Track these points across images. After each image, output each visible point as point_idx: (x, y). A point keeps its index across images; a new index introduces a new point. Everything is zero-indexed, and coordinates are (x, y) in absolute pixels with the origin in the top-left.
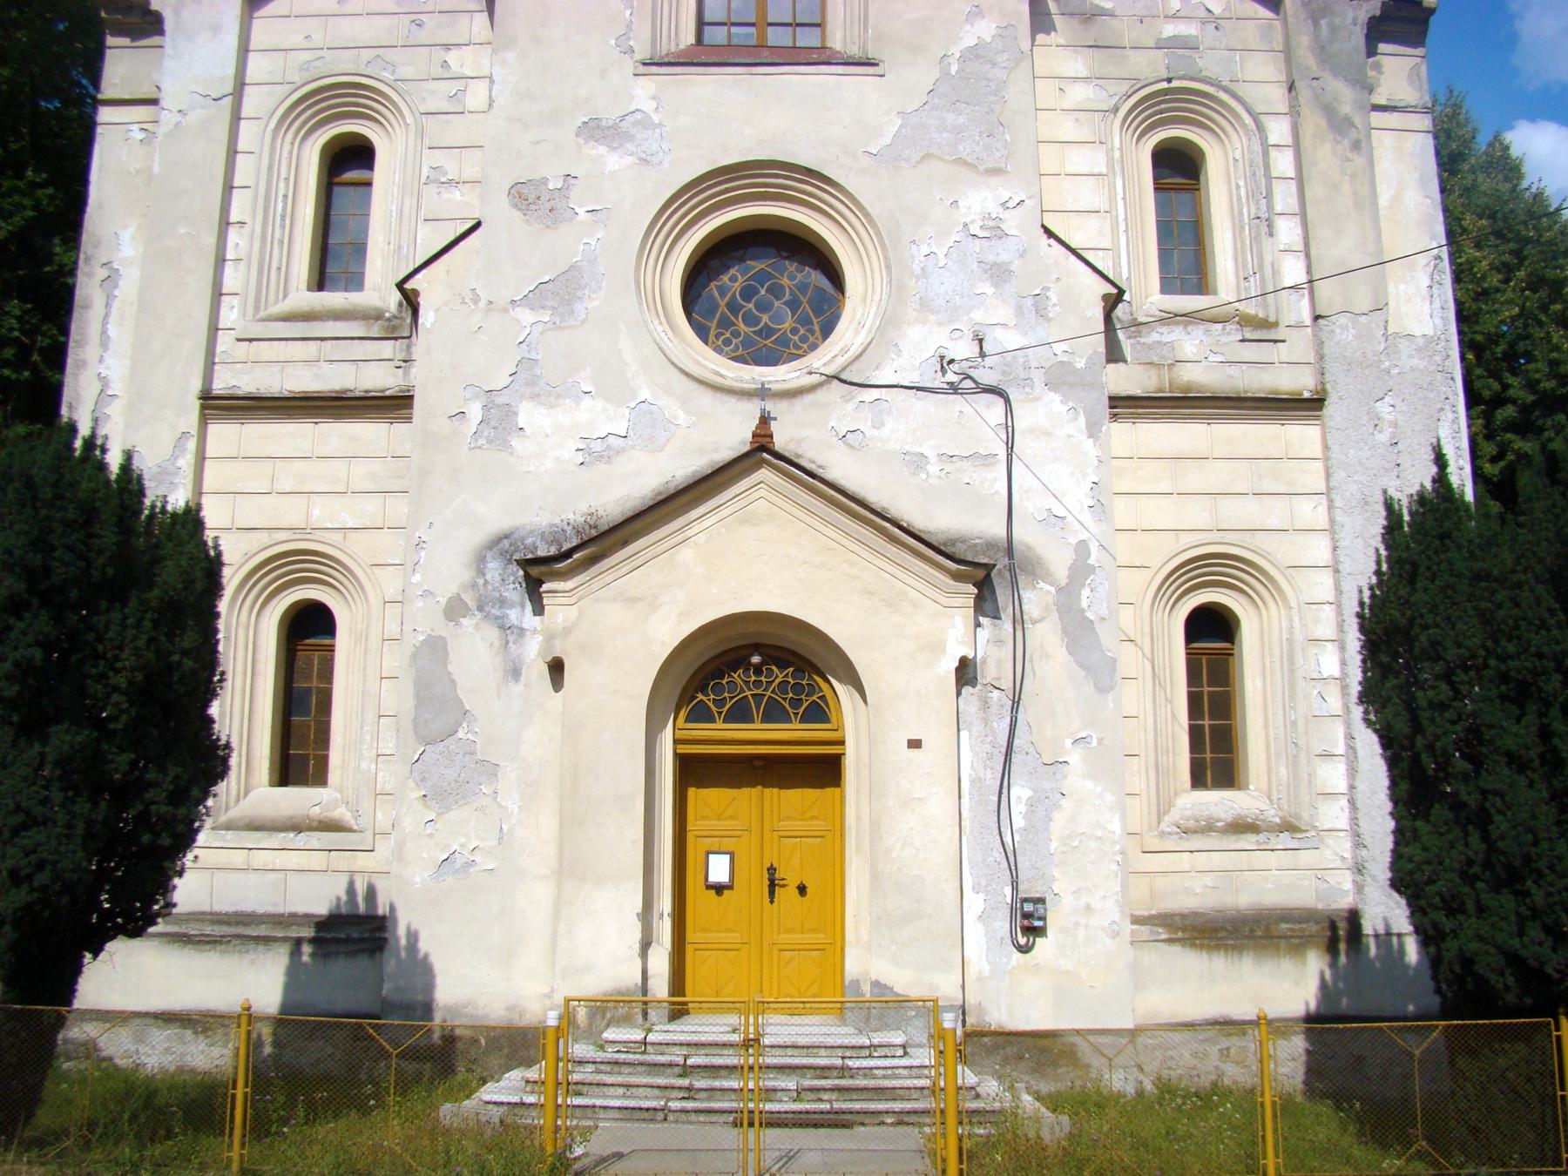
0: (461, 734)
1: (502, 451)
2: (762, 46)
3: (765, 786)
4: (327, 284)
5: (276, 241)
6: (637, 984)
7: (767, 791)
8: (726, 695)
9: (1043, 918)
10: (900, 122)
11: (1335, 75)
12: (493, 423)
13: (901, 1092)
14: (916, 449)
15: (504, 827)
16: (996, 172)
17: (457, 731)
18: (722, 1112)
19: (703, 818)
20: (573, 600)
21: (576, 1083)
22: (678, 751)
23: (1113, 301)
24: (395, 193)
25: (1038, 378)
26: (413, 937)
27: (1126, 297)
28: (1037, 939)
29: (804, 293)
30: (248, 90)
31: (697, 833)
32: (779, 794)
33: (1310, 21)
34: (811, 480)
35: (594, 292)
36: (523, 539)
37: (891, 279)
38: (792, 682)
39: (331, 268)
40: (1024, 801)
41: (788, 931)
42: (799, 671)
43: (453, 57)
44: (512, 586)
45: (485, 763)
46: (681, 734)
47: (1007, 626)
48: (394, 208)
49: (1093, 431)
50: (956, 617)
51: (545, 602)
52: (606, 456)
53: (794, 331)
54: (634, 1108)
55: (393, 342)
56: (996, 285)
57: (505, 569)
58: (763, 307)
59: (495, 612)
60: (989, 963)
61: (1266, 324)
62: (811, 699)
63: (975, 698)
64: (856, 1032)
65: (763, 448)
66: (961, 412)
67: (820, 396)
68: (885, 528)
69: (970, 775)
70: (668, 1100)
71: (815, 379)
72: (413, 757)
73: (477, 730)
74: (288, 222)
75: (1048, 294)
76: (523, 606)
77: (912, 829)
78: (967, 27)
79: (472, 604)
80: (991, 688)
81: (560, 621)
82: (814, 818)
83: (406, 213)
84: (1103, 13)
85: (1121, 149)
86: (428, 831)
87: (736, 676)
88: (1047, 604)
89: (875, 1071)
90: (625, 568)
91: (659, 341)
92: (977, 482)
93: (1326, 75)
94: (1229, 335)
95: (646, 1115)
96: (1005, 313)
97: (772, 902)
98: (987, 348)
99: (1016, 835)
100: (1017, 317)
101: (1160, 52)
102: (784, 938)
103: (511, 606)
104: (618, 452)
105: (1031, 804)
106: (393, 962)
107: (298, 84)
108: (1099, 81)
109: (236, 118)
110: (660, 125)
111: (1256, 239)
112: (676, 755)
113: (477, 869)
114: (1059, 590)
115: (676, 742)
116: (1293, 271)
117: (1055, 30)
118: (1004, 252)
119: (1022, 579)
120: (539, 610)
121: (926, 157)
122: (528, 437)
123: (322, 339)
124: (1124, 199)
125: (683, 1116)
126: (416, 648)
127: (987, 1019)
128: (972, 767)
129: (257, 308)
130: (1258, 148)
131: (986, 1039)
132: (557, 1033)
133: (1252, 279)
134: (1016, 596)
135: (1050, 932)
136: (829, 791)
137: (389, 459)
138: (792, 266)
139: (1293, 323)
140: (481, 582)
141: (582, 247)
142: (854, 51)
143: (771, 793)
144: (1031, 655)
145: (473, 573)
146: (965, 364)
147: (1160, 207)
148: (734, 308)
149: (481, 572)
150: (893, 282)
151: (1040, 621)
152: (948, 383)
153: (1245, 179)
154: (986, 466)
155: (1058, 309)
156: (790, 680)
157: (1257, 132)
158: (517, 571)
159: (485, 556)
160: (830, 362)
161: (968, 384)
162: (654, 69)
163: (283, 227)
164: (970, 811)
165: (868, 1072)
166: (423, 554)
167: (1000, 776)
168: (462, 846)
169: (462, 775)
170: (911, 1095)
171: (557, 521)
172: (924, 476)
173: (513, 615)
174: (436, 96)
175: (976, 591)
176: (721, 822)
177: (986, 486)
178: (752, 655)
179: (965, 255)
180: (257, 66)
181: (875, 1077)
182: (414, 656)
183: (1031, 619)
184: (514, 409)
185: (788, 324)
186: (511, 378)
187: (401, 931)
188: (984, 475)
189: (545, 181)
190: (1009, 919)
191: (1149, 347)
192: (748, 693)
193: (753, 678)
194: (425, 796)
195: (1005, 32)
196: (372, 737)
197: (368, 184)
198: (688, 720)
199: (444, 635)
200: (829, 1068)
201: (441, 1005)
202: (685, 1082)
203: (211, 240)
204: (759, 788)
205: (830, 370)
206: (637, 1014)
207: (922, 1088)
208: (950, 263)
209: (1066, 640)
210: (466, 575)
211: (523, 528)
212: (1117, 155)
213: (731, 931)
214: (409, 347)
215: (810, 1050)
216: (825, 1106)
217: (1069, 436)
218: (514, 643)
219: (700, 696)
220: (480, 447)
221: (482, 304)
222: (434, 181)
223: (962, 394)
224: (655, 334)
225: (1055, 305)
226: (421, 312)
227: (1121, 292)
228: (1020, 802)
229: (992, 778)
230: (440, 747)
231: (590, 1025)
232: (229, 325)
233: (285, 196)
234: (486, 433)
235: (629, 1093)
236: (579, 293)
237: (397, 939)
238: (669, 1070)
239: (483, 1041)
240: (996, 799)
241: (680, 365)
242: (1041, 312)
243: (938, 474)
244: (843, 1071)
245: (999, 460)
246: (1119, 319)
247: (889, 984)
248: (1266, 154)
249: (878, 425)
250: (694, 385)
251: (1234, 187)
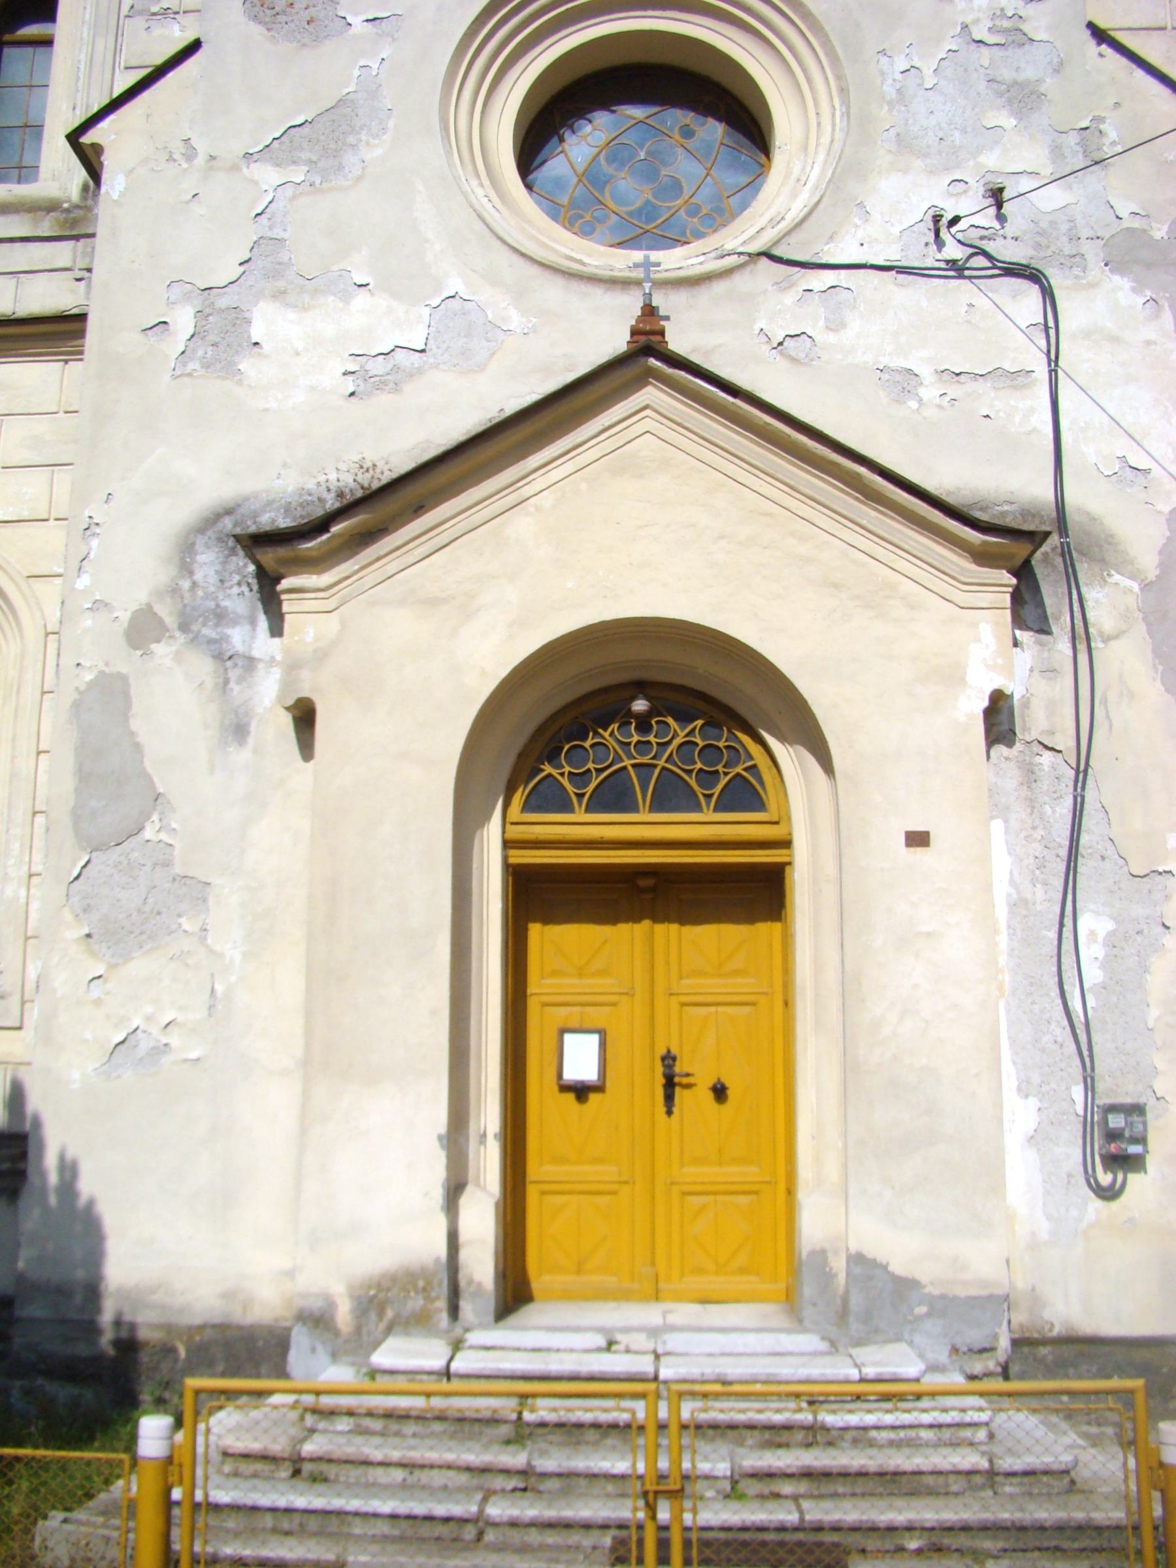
0: (149, 833)
1: (224, 378)
3: (656, 919)
7: (660, 928)
8: (591, 765)
9: (1142, 1140)
13: (929, 1480)
17: (141, 829)
18: (587, 1526)
20: (331, 604)
22: (512, 860)
24: (85, 35)
25: (1093, 253)
26: (69, 1171)
28: (1130, 1176)
32: (680, 934)
34: (730, 399)
35: (375, 136)
37: (848, 107)
38: (701, 744)
40: (1100, 938)
42: (711, 723)
44: (236, 590)
45: (189, 881)
46: (515, 832)
48: (83, 57)
51: (286, 607)
52: (392, 382)
55: (71, 243)
56: (1019, 115)
57: (224, 563)
59: (209, 632)
60: (1049, 1218)
62: (734, 771)
63: (1012, 764)
64: (823, 1346)
65: (649, 350)
67: (742, 282)
68: (858, 476)
69: (1009, 895)
70: (488, 1494)
72: (70, 872)
73: (174, 825)
75: (1102, 127)
77: (916, 986)
79: (170, 621)
80: (1037, 748)
82: (737, 973)
83: (98, 58)
87: (606, 735)
88: (1127, 609)
89: (873, 1433)
91: (477, 207)
92: (1001, 414)
97: (669, 1112)
99: (1089, 997)
100: (1054, 162)
103: (235, 622)
104: (411, 376)
105: (1113, 943)
106: (36, 1213)
114: (1146, 587)
115: (507, 844)
119: (1082, 568)
122: (266, 356)
126: (80, 693)
127: (1047, 1314)
128: (1012, 881)
131: (1043, 1351)
132: (165, 1473)
135: (1151, 1162)
137: (61, 415)
140: (186, 584)
141: (356, 73)
143: (667, 933)
145: (173, 571)
150: (852, 111)
151: (1116, 637)
152: (947, 262)
154: (1015, 388)
156: (698, 740)
158: (245, 566)
159: (193, 544)
160: (752, 238)
164: (1010, 955)
165: (860, 1436)
166: (95, 543)
169: (151, 900)
170: (947, 1485)
171: (311, 485)
172: (913, 404)
173: (237, 637)
178: (633, 698)
179: (966, 70)
182: (77, 705)
183: (1101, 633)
184: (247, 315)
186: (242, 269)
187: (51, 1161)
188: (1013, 403)
190: (1080, 1142)
192: (627, 763)
193: (636, 738)
194: (89, 936)
196: (22, 845)
198: (527, 807)
200: (788, 1427)
202: (516, 1458)
204: (646, 923)
206: (441, 1310)
207: (970, 1473)
208: (943, 83)
209: (1160, 668)
210: (163, 575)
211: (256, 497)
216: (792, 1517)
217: (1148, 343)
218: (239, 682)
219: (548, 769)
220: (189, 375)
221: (200, 160)
222: (142, 13)
223: (970, 278)
224: (472, 197)
226: (105, 177)
228: (1095, 941)
229: (1046, 900)
230: (115, 854)
231: (358, 1330)
234: (200, 353)
236: (351, 139)
237: (43, 1175)
238: (490, 1431)
239: (182, 1352)
243: (938, 401)
244: (815, 1434)
245: (1036, 380)
247: (881, 1257)
249: (836, 325)
250: (535, 270)
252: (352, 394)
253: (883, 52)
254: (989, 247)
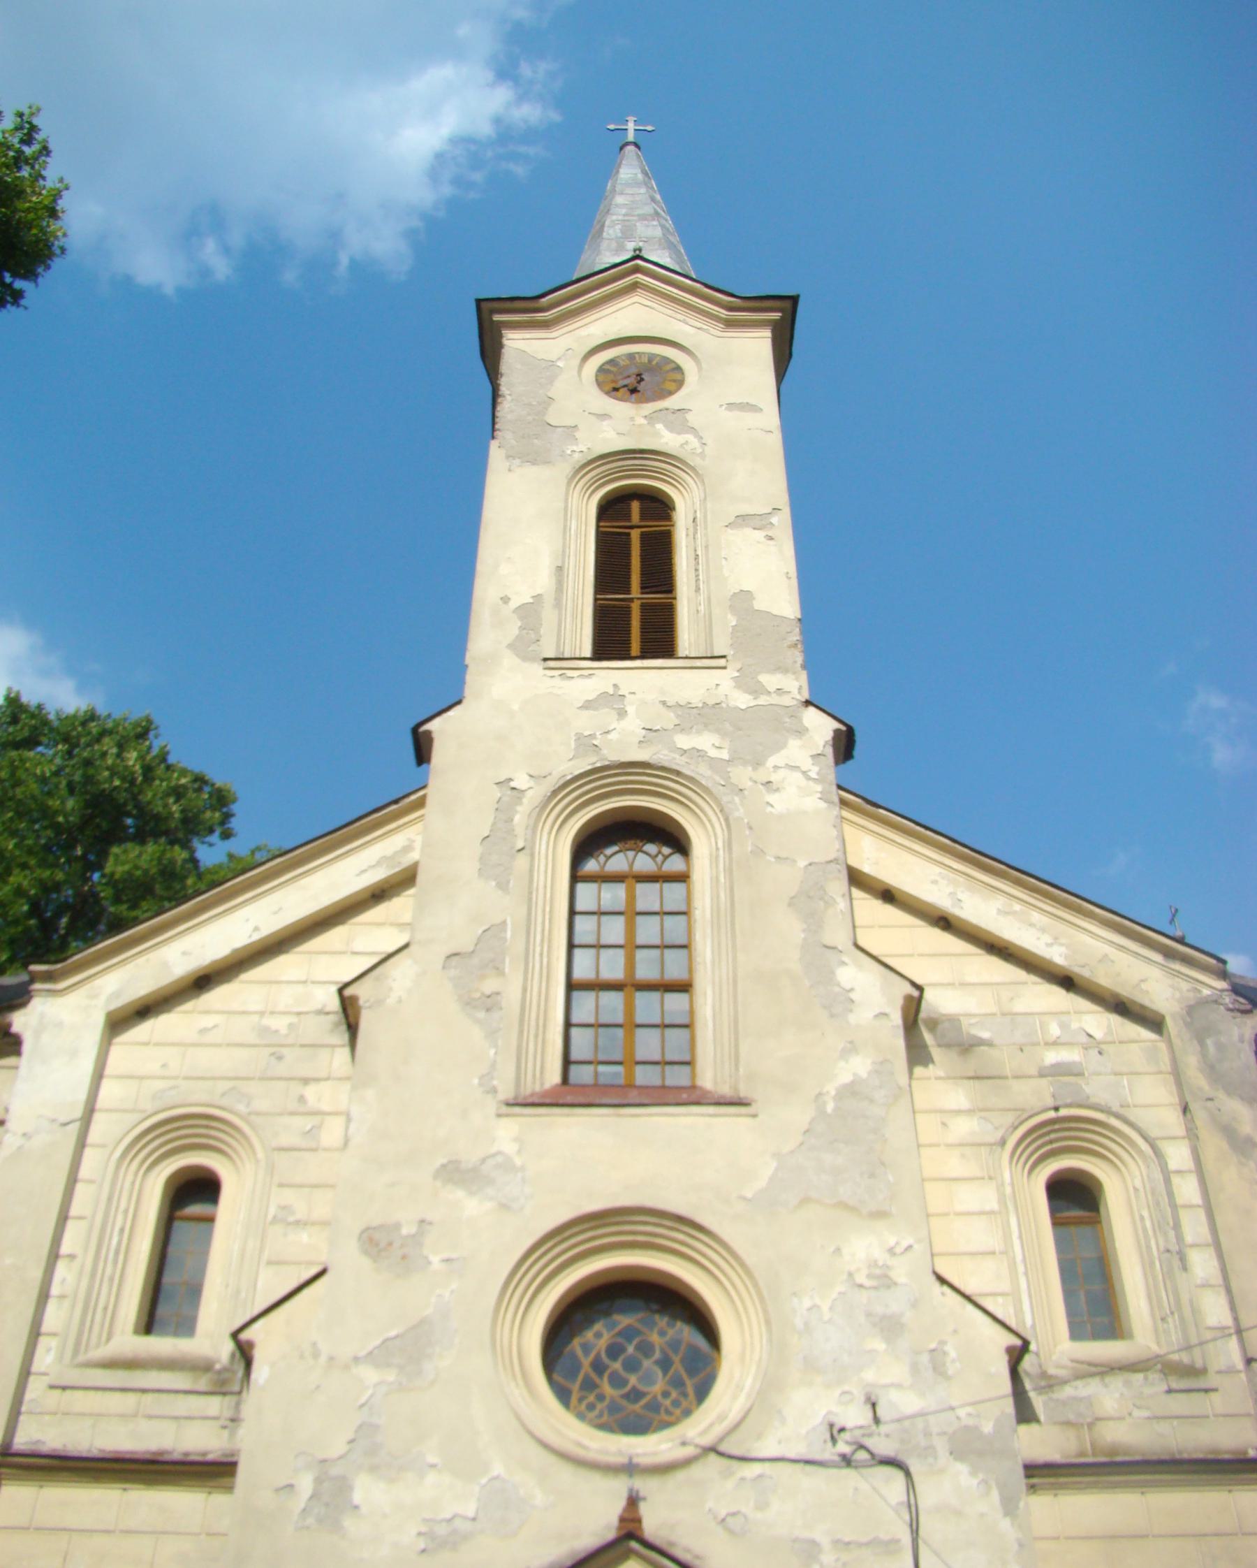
2: (630, 1086)
4: (156, 1326)
5: (106, 1279)
10: (774, 1164)
11: (1229, 1094)
14: (806, 1534)
16: (880, 1215)
23: (1017, 1355)
25: (941, 1446)
27: (1033, 1347)
29: (676, 1351)
30: (97, 1117)
33: (1195, 1042)
39: (162, 1310)
43: (311, 1092)
49: (1009, 1507)
53: (666, 1394)
58: (632, 1366)
61: (1191, 1371)
67: (696, 1471)
71: (689, 1451)
74: (121, 1257)
78: (842, 1064)
84: (982, 1042)
85: (1012, 1185)
93: (1221, 1095)
94: (1152, 1386)
96: (897, 1371)
98: (880, 1412)
101: (1044, 1082)
107: (148, 1113)
108: (983, 1114)
109: (81, 1144)
110: (523, 1168)
111: (1168, 1274)
116: (1215, 1311)
117: (933, 1062)
118: (895, 1303)
121: (805, 1201)
123: (144, 1391)
124: (1020, 1237)
129: (76, 1351)
130: (1158, 1176)
133: (1170, 1320)
138: (662, 1321)
139: (1223, 1368)
142: (725, 1090)
146: (858, 1433)
147: (1062, 1245)
148: (598, 1367)
153: (1149, 1207)
155: (958, 1365)
157: (1155, 1159)
161: (862, 1455)
162: (517, 1110)
163: (115, 1262)
174: (291, 1130)
180: (110, 1091)
185: (658, 1387)
189: (397, 1226)
191: (1064, 1403)
195: (881, 1068)
197: (211, 1220)
203: (37, 1273)
205: (707, 1440)
212: (1008, 1190)
214: (238, 1406)
217: (982, 1515)
221: (323, 1359)
225: (953, 1361)
227: (1025, 1345)
232: (43, 1369)
233: (122, 1230)
241: (537, 1433)
242: (939, 1369)
246: (1028, 1374)
248: (1167, 1181)
249: (762, 1506)
250: (551, 1459)
251: (1137, 1218)
252: (423, 1551)
253: (794, 1294)
254: (869, 1442)
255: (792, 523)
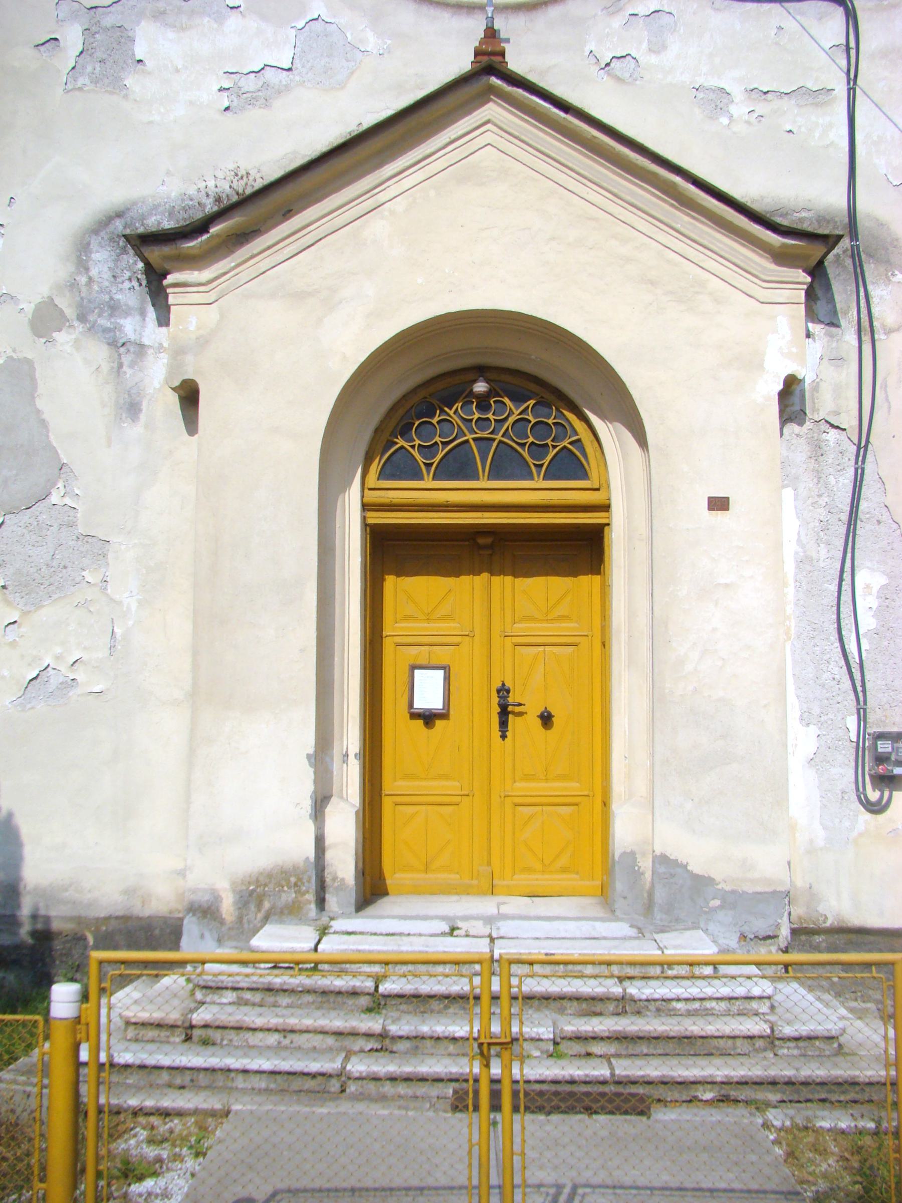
0: (55, 498)
6: (307, 858)
7: (497, 580)
8: (437, 439)
12: (99, 55)
15: (116, 630)
19: (407, 618)
20: (212, 296)
21: (206, 1026)
22: (370, 521)
28: (894, 793)
31: (397, 639)
34: (562, 114)
36: (143, 218)
38: (533, 421)
40: (875, 591)
41: (528, 778)
45: (90, 540)
46: (373, 497)
47: (850, 337)
50: (779, 318)
51: (171, 300)
54: (289, 1073)
57: (116, 261)
59: (104, 322)
60: (825, 828)
64: (633, 932)
66: (780, 28)
68: (674, 185)
69: (796, 553)
73: (77, 492)
76: (143, 313)
77: (714, 630)
79: (70, 312)
80: (824, 426)
81: (192, 328)
86: (10, 638)
87: (451, 412)
90: (288, 249)
92: (803, 129)
95: (310, 1084)
97: (504, 737)
99: (863, 641)
102: (522, 787)
103: (127, 313)
104: (279, 92)
112: (365, 525)
113: (79, 691)
115: (365, 507)
120: (164, 320)
122: (149, 73)
125: (371, 1087)
127: (821, 909)
132: (74, 1032)
134: (862, 293)
136: (584, 580)
140: (83, 280)
143: (502, 584)
144: (885, 379)
145: (71, 268)
149: (83, 265)
156: (531, 418)
158: (135, 263)
159: (89, 244)
164: (796, 604)
165: (663, 1006)
167: (840, 554)
168: (58, 658)
170: (735, 1048)
171: (192, 191)
172: (725, 121)
173: (129, 326)
175: (809, 279)
176: (431, 625)
177: (817, 135)
178: (475, 381)
181: (673, 1013)
183: (883, 326)
184: (130, 34)
190: (853, 764)
192: (470, 437)
198: (382, 475)
199: (30, 356)
201: (30, 887)
202: (374, 1024)
204: (485, 575)
210: (62, 271)
213: (446, 777)
215: (570, 967)
216: (601, 1071)
218: (131, 366)
219: (401, 442)
220: (80, 89)
230: (26, 517)
231: (240, 919)
234: (89, 69)
235: (286, 1042)
238: (351, 1002)
240: (834, 588)
243: (746, 117)
247: (682, 859)
249: (657, 48)
252: (227, 109)
255: (437, 316)
